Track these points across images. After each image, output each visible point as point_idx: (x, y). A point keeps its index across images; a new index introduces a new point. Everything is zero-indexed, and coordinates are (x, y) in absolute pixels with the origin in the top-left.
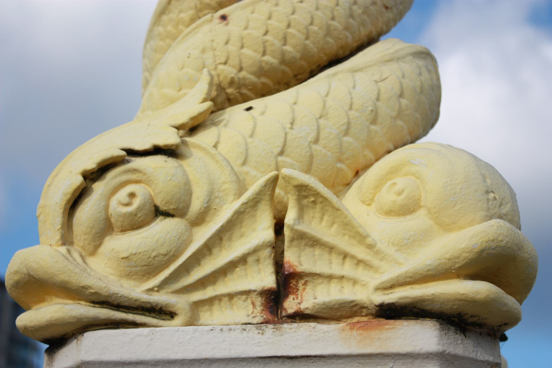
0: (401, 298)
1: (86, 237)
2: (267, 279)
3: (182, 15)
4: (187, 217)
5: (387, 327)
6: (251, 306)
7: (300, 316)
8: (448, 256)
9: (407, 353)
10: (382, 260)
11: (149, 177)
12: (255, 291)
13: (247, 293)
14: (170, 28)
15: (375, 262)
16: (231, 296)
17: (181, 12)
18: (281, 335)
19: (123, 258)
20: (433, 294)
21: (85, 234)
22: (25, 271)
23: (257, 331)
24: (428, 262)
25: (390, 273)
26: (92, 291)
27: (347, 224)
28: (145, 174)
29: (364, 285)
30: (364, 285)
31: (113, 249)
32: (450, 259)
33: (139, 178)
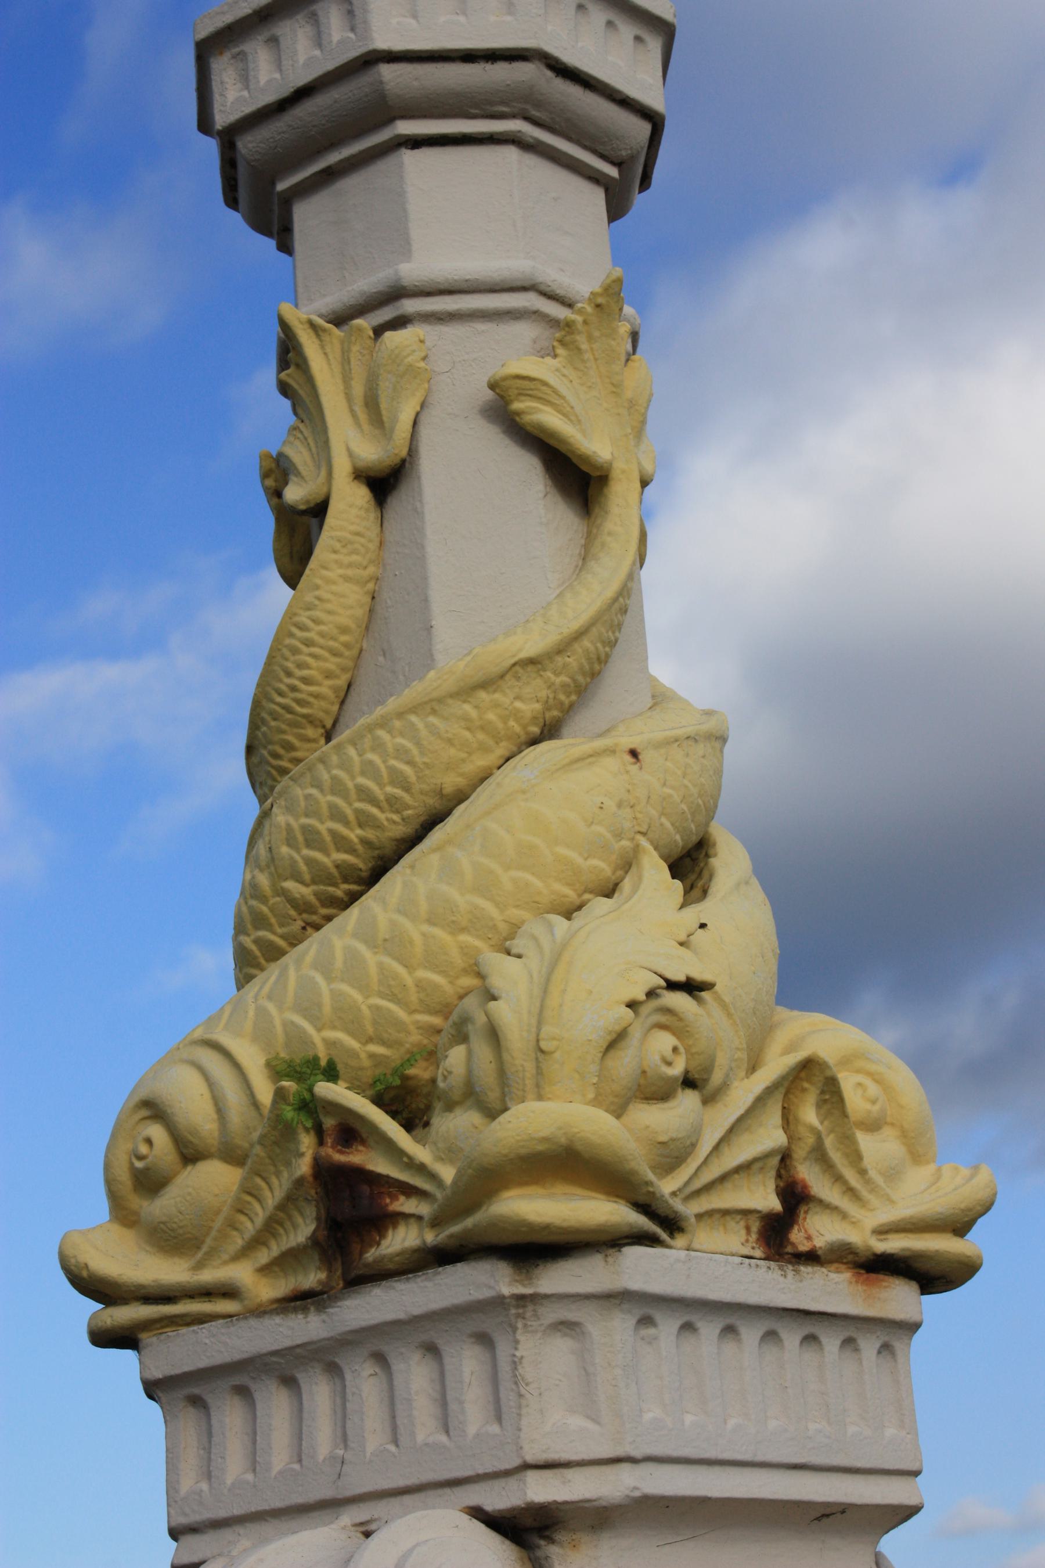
0: (903, 1250)
1: (616, 1100)
2: (766, 1199)
3: (518, 704)
4: (705, 1092)
5: (884, 1284)
6: (743, 1232)
7: (811, 1257)
8: (963, 1206)
9: (902, 1322)
10: (871, 1191)
11: (687, 1026)
12: (758, 1212)
13: (746, 1213)
14: (491, 716)
15: (864, 1193)
16: (726, 1213)
17: (518, 698)
18: (801, 1281)
19: (659, 1143)
20: (937, 1251)
21: (616, 1096)
22: (563, 1140)
23: (780, 1272)
24: (939, 1209)
25: (886, 1215)
26: (651, 1189)
27: (847, 1138)
28: (681, 1020)
29: (853, 1223)
30: (853, 1223)
31: (647, 1127)
32: (963, 1211)
33: (668, 1023)
